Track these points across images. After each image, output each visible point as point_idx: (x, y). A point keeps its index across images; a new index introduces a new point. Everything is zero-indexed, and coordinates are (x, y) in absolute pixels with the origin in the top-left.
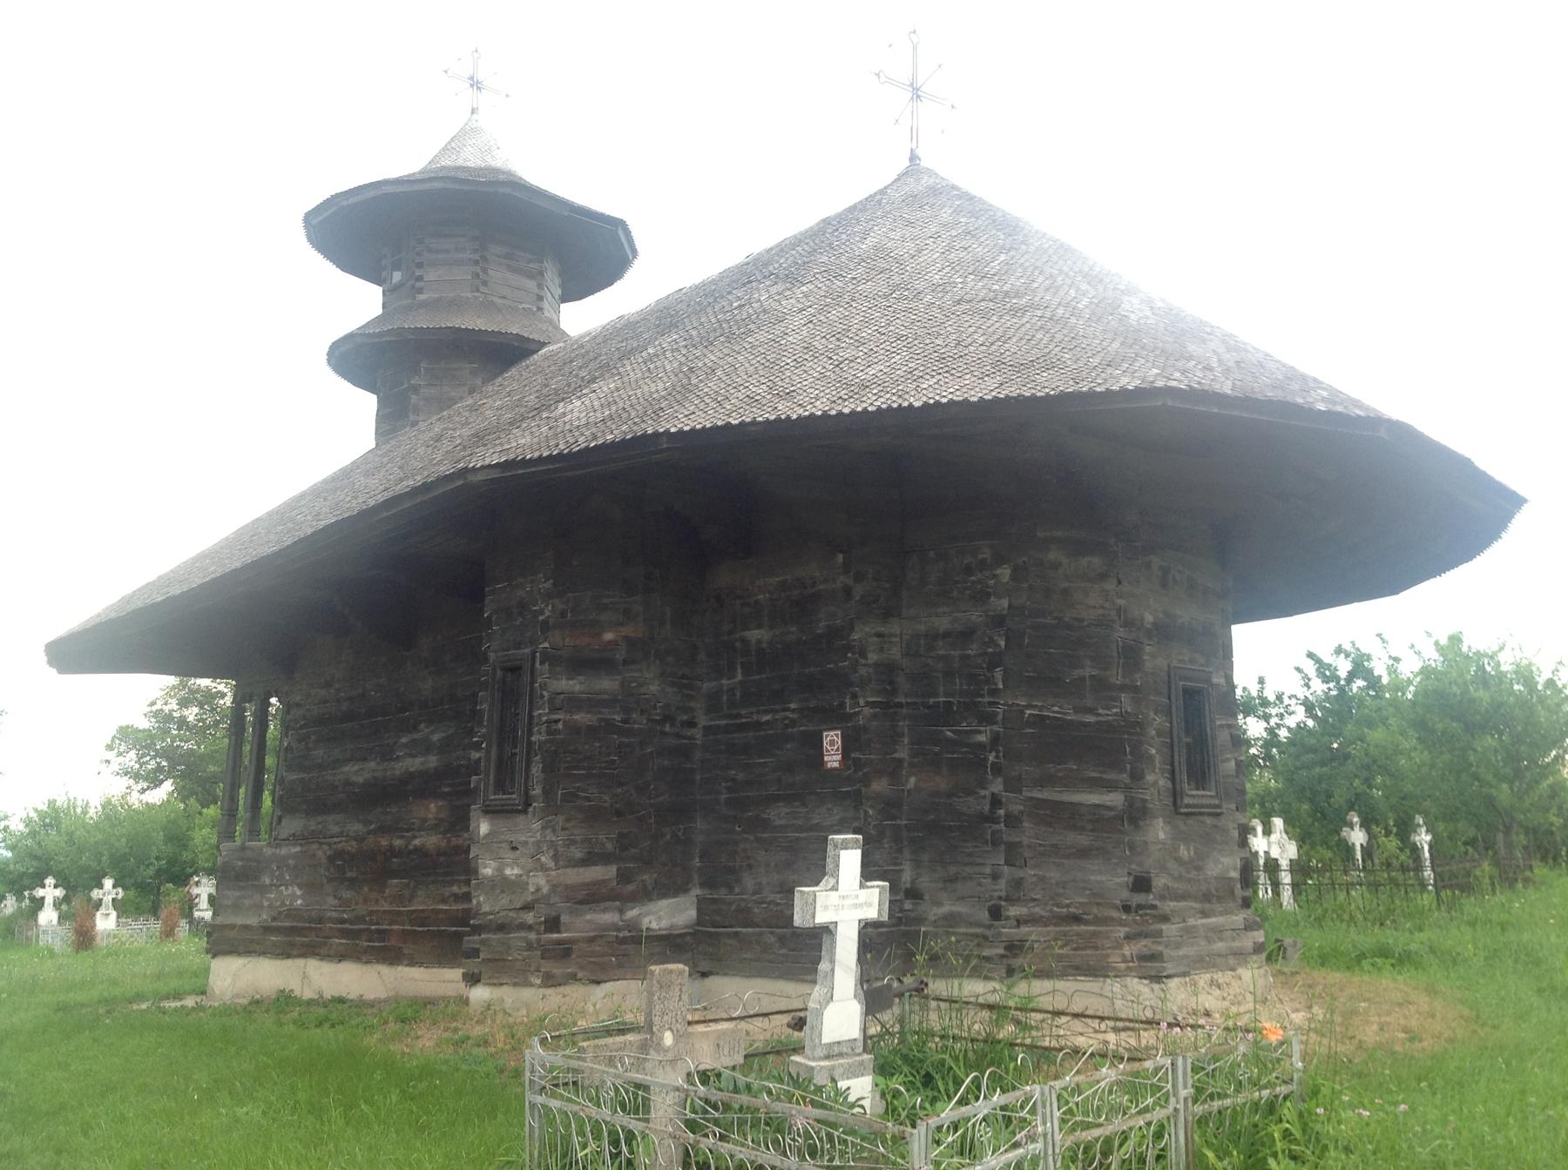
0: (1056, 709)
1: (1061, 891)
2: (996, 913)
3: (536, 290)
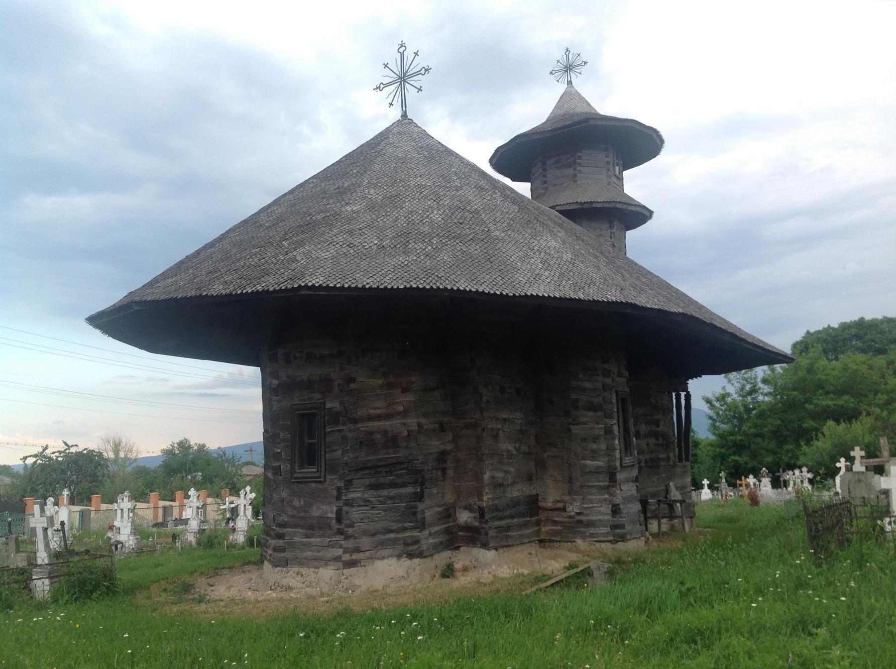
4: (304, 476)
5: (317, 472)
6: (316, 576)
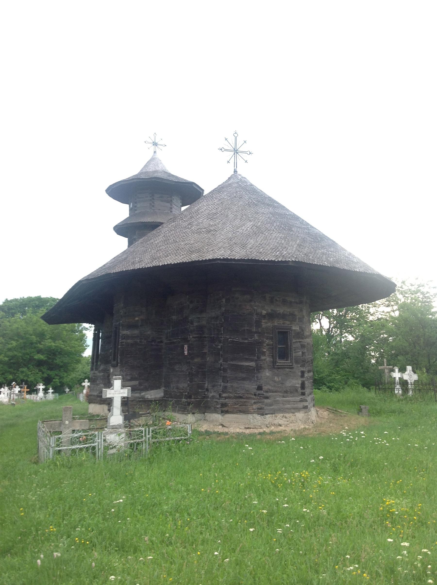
0: (237, 339)
1: (237, 389)
2: (220, 395)
3: (170, 206)
4: (283, 364)
5: (291, 362)
6: (295, 417)
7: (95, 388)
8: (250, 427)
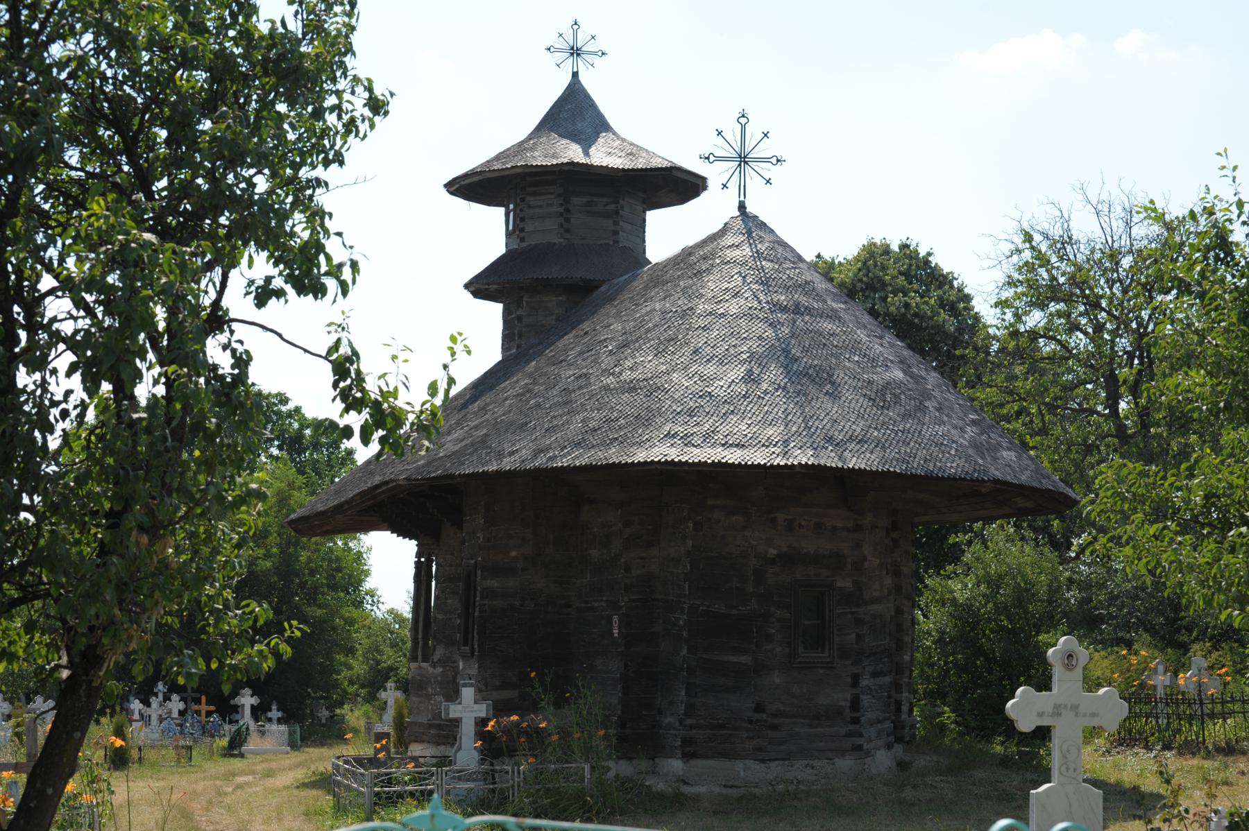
7: (423, 706)
8: (735, 784)
